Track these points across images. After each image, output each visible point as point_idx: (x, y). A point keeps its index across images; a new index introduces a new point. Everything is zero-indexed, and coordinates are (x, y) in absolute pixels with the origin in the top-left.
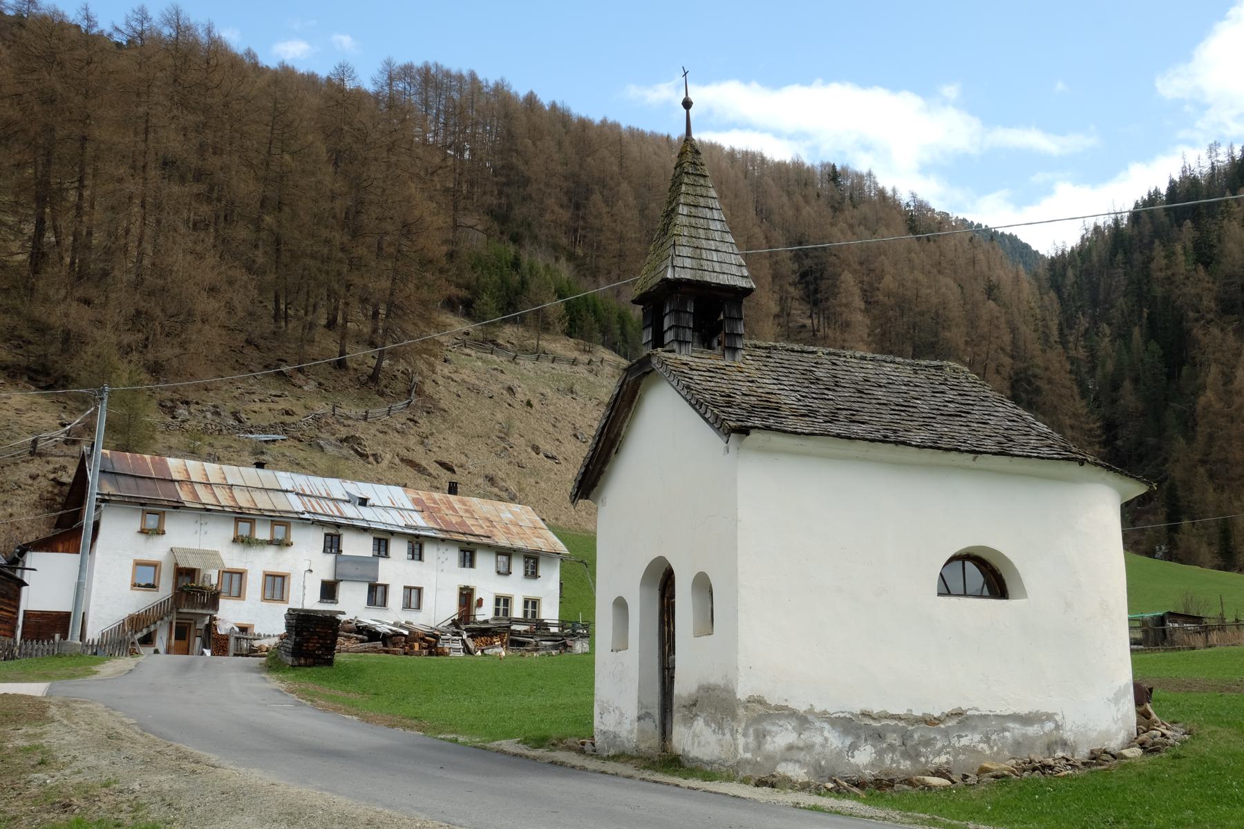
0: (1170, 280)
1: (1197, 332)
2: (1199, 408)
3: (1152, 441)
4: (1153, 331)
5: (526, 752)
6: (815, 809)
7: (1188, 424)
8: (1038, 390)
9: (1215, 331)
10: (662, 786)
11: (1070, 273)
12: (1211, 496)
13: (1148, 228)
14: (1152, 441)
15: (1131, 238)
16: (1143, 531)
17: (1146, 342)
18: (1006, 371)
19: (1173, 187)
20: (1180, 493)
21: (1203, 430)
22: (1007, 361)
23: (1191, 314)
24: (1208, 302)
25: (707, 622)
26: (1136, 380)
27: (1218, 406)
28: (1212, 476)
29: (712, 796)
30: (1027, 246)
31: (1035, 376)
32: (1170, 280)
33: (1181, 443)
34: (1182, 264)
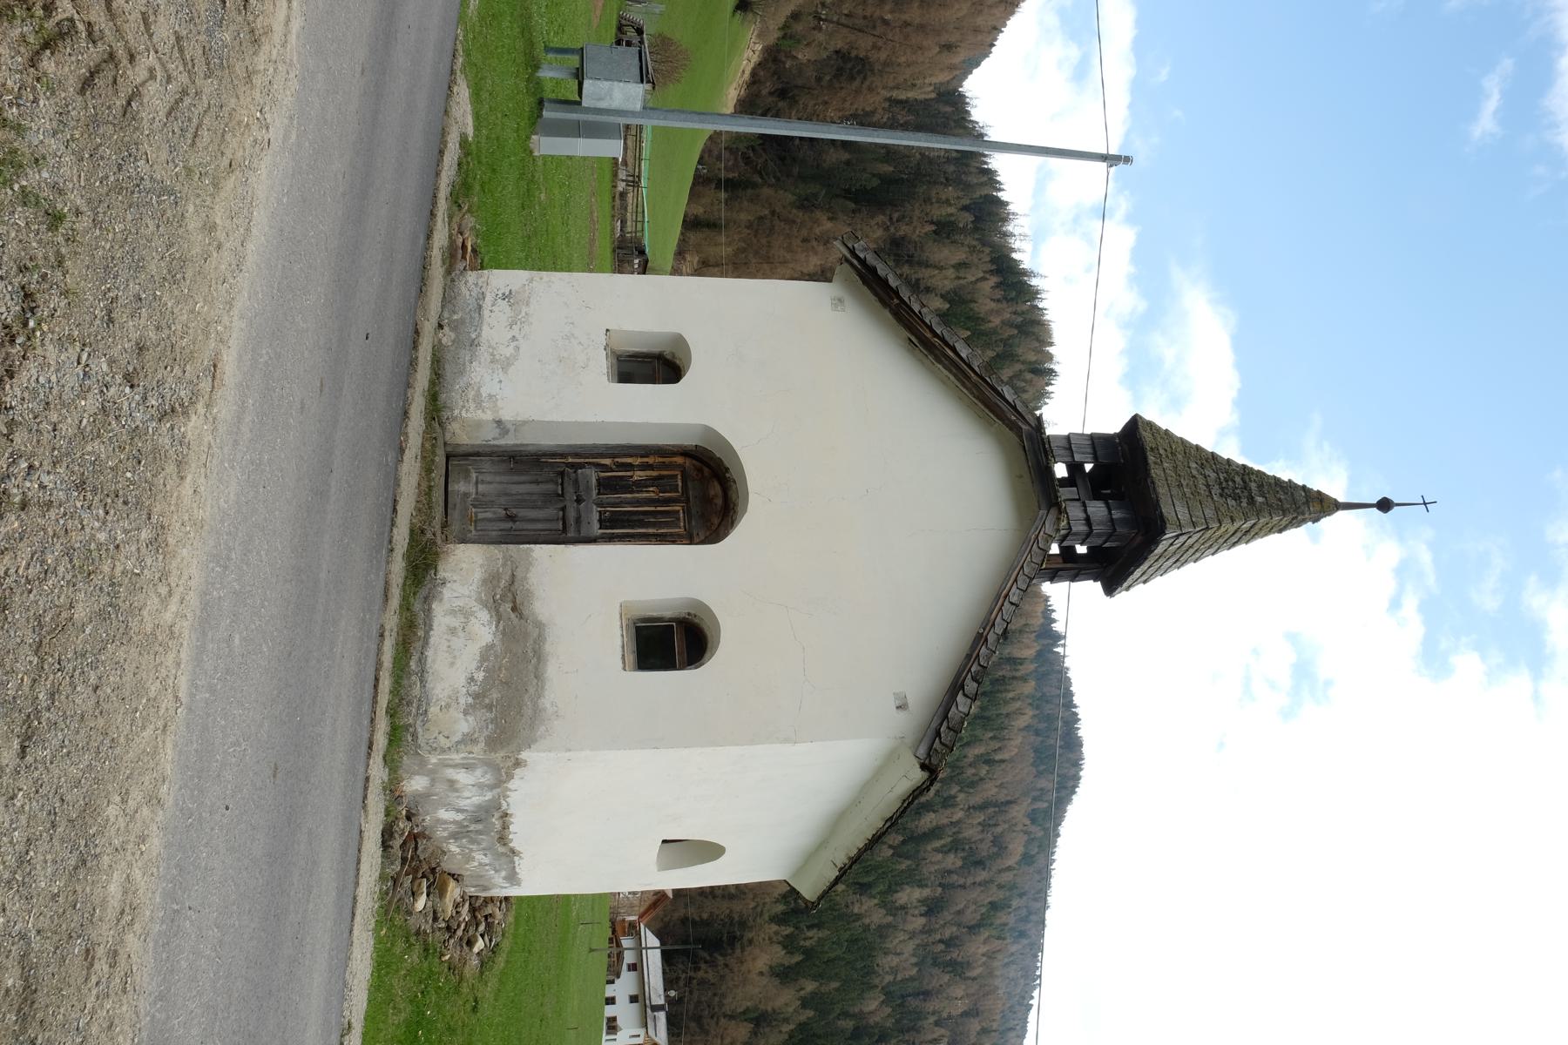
0: (927, 200)
1: (880, 218)
2: (818, 214)
3: (796, 170)
4: (887, 181)
5: (444, 175)
6: (379, 666)
7: (806, 204)
8: (852, 78)
9: (879, 233)
10: (367, 707)
11: (949, 109)
12: (744, 217)
13: (974, 180)
14: (796, 170)
15: (967, 165)
16: (719, 158)
17: (879, 176)
18: (874, 56)
19: (1004, 204)
20: (749, 191)
21: (799, 215)
22: (883, 56)
23: (896, 216)
24: (904, 229)
25: (709, 851)
26: (848, 163)
27: (817, 231)
28: (761, 218)
29: (353, 851)
30: (978, 65)
31: (865, 78)
32: (927, 200)
33: (790, 198)
34: (939, 212)
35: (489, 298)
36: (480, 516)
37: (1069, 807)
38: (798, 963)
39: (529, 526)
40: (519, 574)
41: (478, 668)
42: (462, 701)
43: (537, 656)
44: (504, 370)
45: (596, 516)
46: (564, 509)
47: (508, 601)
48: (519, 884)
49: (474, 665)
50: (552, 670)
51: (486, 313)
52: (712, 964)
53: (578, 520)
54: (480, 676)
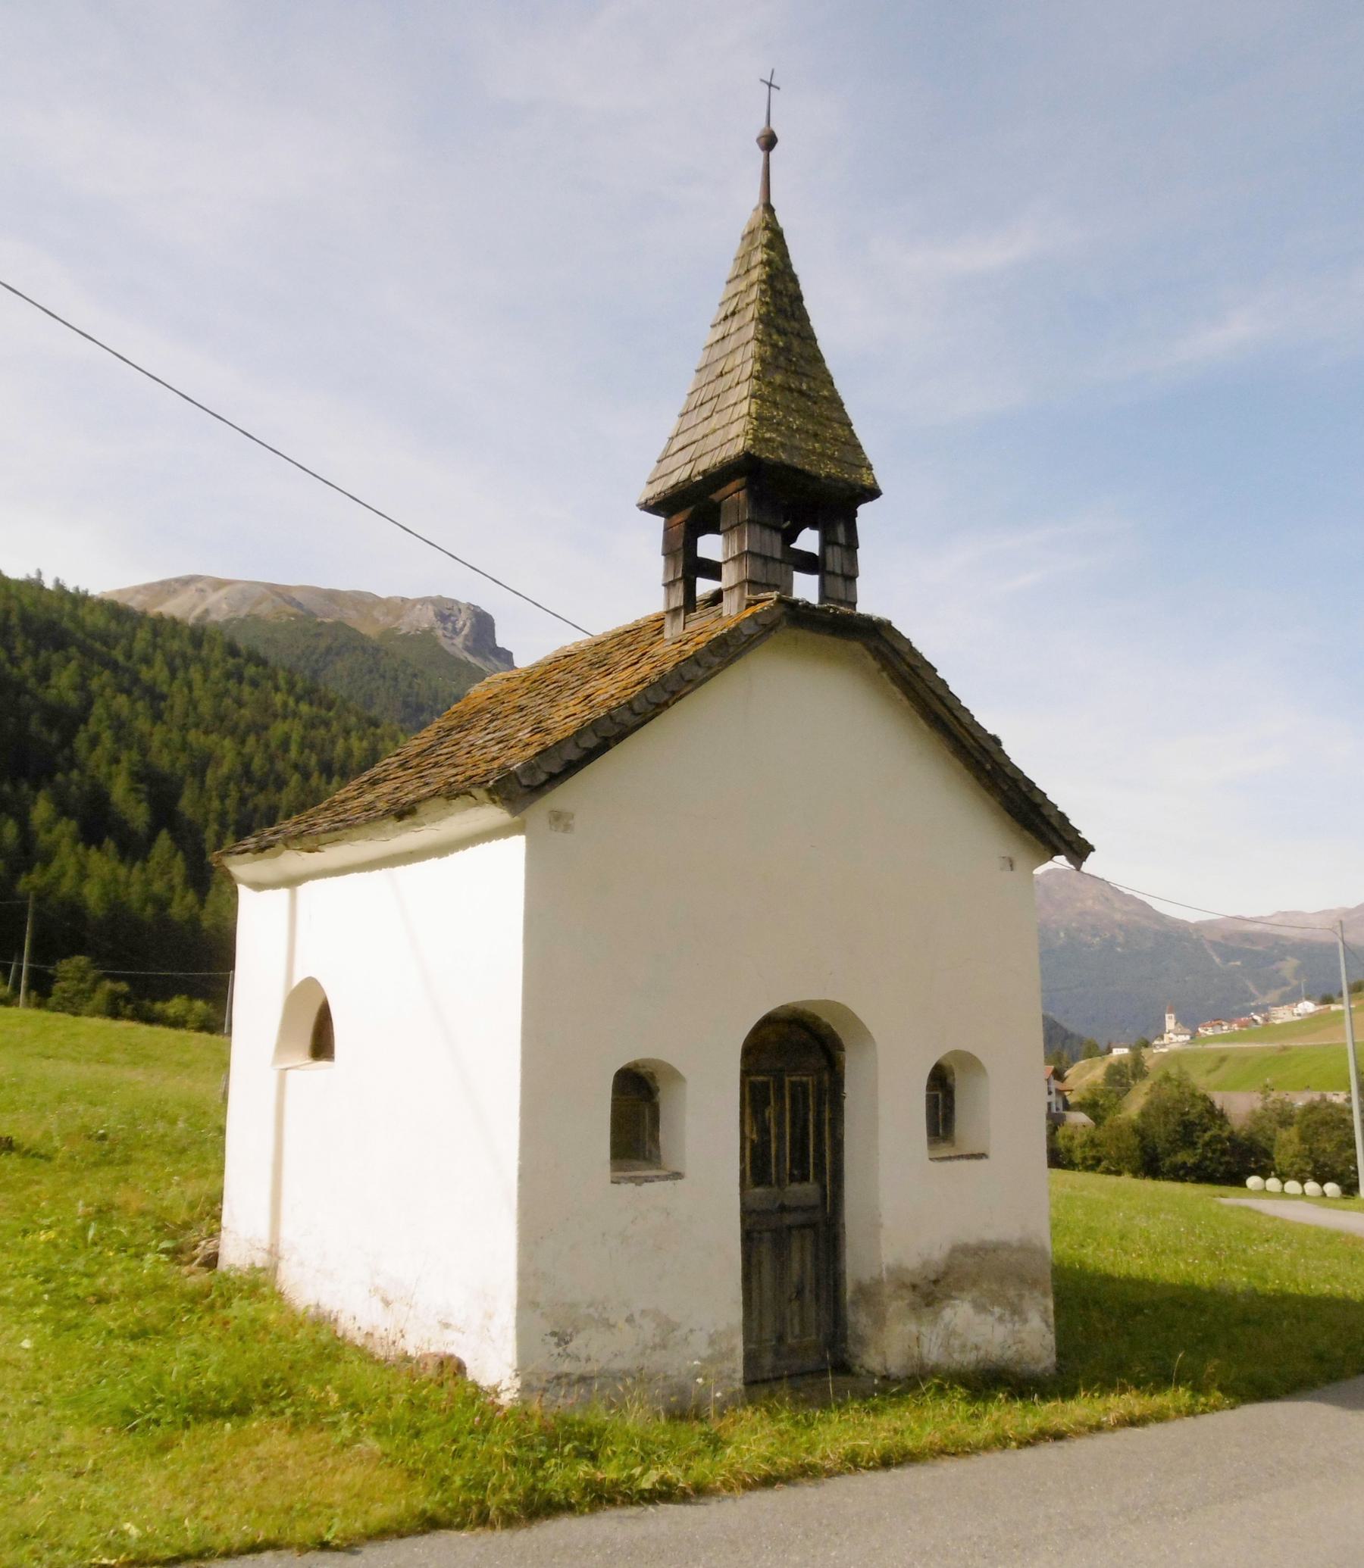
35: (566, 1367)
36: (797, 1330)
37: (857, 519)
38: (1020, 790)
39: (809, 1266)
40: (908, 1279)
41: (992, 1314)
42: (1017, 1326)
43: (982, 1252)
44: (674, 1327)
45: (796, 1187)
46: (790, 1228)
47: (930, 1291)
48: (953, 1143)
49: (990, 1319)
50: (991, 1235)
51: (593, 1368)
52: (1263, 1129)
53: (804, 1209)
54: (997, 1310)
